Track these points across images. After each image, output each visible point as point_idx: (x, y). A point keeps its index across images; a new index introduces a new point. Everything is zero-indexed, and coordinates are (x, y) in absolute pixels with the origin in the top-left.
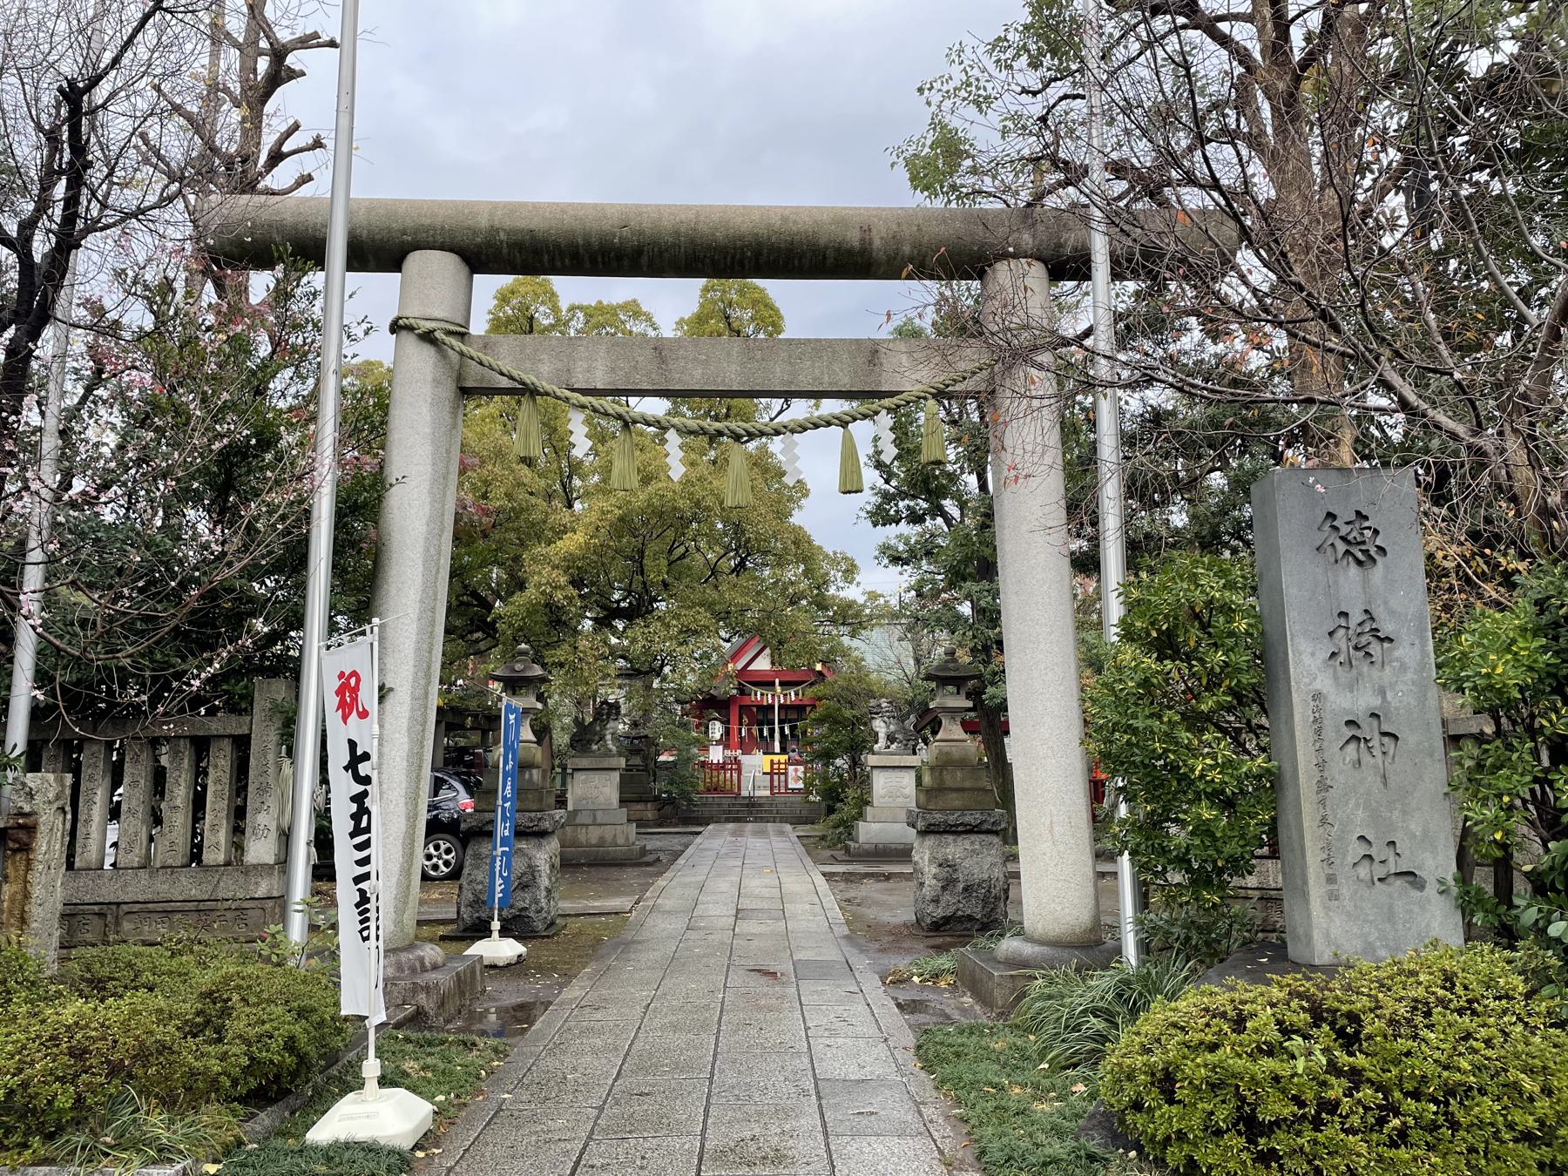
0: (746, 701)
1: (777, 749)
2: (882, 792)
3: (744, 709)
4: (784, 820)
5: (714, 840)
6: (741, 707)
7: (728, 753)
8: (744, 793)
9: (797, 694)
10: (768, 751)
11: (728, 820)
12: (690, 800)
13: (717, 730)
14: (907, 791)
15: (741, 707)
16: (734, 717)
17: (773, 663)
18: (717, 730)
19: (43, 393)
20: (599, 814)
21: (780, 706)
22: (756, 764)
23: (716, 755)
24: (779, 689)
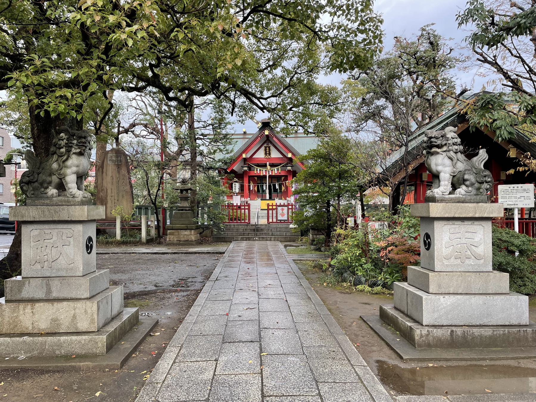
0: (252, 174)
1: (268, 197)
2: (445, 252)
3: (252, 178)
4: (276, 239)
5: (236, 249)
6: (250, 177)
7: (243, 199)
8: (253, 221)
9: (278, 170)
10: (263, 199)
11: (242, 239)
12: (219, 229)
13: (236, 187)
14: (480, 250)
15: (250, 177)
16: (246, 180)
17: (266, 154)
18: (236, 187)
19: (45, 93)
20: (55, 285)
21: (269, 176)
22: (257, 205)
23: (237, 200)
24: (269, 167)
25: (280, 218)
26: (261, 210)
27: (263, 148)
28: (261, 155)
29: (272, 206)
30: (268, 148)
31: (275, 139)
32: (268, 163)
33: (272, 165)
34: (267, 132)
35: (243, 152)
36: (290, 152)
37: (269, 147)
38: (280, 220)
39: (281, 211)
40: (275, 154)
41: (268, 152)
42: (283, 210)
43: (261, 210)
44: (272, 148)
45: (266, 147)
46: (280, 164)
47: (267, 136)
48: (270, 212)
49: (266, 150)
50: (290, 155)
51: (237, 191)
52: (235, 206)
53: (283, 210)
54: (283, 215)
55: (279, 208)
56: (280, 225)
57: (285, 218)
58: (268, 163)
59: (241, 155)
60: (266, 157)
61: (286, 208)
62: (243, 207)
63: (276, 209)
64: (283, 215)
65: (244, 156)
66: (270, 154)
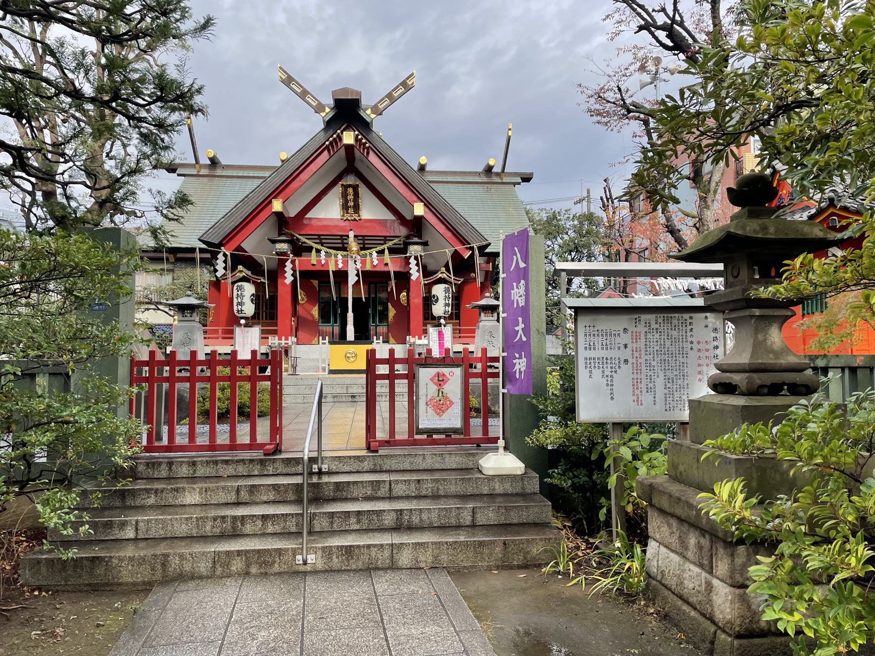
17: (345, 207)
25: (427, 420)
26: (332, 372)
27: (338, 190)
28: (330, 211)
29: (391, 361)
30: (350, 190)
31: (373, 158)
32: (351, 234)
33: (365, 244)
34: (349, 138)
35: (276, 193)
36: (421, 198)
37: (355, 188)
38: (430, 432)
39: (433, 389)
40: (371, 210)
41: (351, 205)
42: (440, 380)
43: (332, 372)
44: (363, 190)
45: (346, 187)
46: (386, 239)
47: (349, 148)
48: (382, 387)
49: (344, 195)
50: (419, 209)
51: (249, 309)
52: (244, 363)
53: (440, 380)
54: (441, 406)
55: (425, 374)
56: (428, 457)
57: (453, 419)
58: (351, 234)
59: (267, 202)
60: (347, 216)
61: (458, 372)
62: (227, 371)
63: (412, 378)
64: (441, 406)
65: (277, 206)
66: (357, 208)
